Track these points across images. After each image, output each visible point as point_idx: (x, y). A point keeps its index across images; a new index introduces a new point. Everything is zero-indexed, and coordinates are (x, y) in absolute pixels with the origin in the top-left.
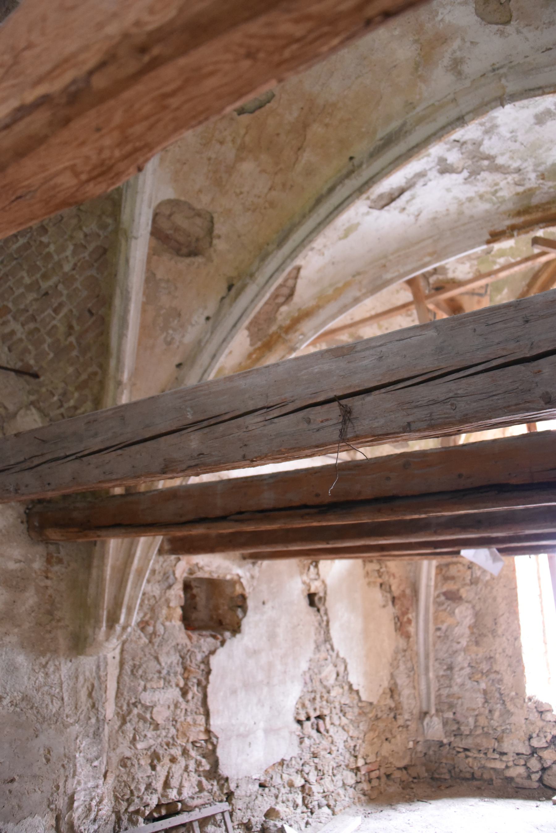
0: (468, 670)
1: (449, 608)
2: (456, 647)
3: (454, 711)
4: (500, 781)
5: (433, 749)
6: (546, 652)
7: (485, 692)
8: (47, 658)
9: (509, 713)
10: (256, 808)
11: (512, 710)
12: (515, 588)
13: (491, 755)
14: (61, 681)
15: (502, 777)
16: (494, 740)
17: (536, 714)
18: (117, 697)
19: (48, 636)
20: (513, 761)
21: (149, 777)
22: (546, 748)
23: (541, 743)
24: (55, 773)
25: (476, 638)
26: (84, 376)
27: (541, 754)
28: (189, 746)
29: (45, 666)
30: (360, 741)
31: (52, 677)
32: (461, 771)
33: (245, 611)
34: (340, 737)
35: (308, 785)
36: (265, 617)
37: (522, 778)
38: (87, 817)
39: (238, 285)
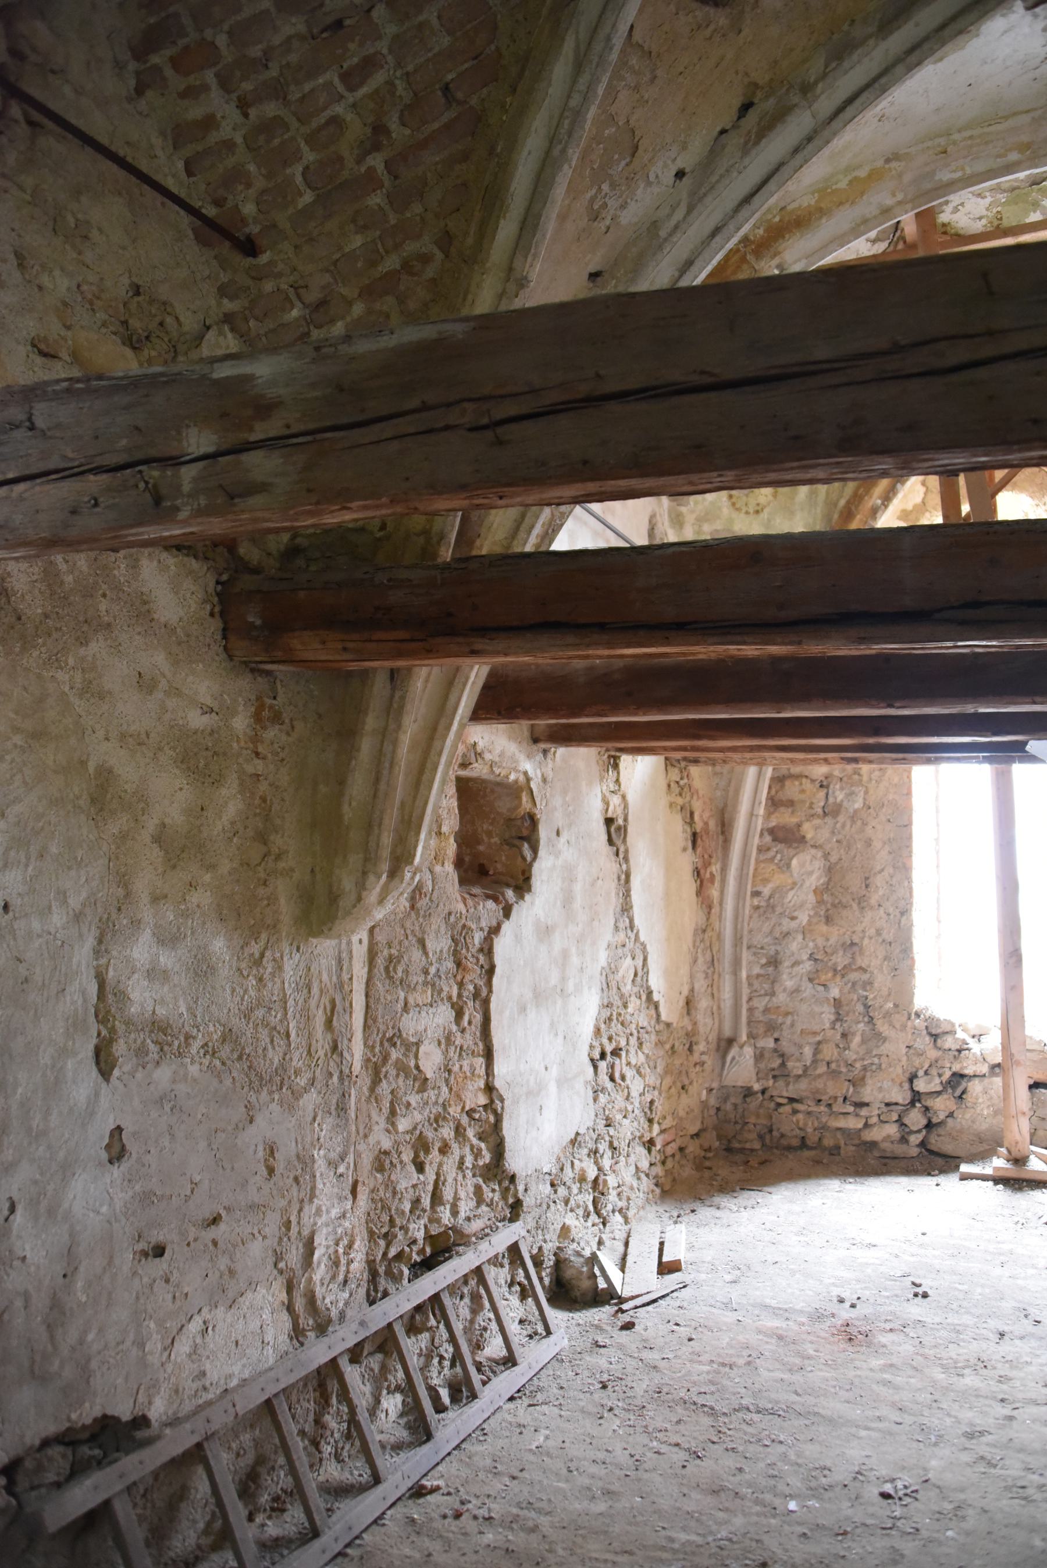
0: (808, 966)
1: (779, 857)
2: (787, 925)
3: (776, 1035)
4: (853, 1148)
5: (733, 1100)
6: (938, 937)
7: (837, 1003)
8: (262, 943)
9: (880, 1038)
10: (550, 1226)
11: (885, 1034)
12: (908, 825)
13: (838, 1107)
14: (285, 995)
15: (857, 1142)
16: (847, 1083)
17: (927, 1038)
18: (366, 1026)
19: (261, 891)
20: (879, 1116)
21: (414, 1186)
22: (939, 1093)
23: (932, 1085)
24: (283, 1197)
25: (827, 910)
26: (391, 263)
27: (929, 1103)
28: (465, 1120)
29: (258, 962)
30: (656, 1093)
31: (270, 985)
32: (782, 1136)
33: (535, 850)
34: (636, 1086)
35: (602, 1177)
36: (560, 862)
37: (892, 1142)
38: (333, 1277)
39: (766, 105)
